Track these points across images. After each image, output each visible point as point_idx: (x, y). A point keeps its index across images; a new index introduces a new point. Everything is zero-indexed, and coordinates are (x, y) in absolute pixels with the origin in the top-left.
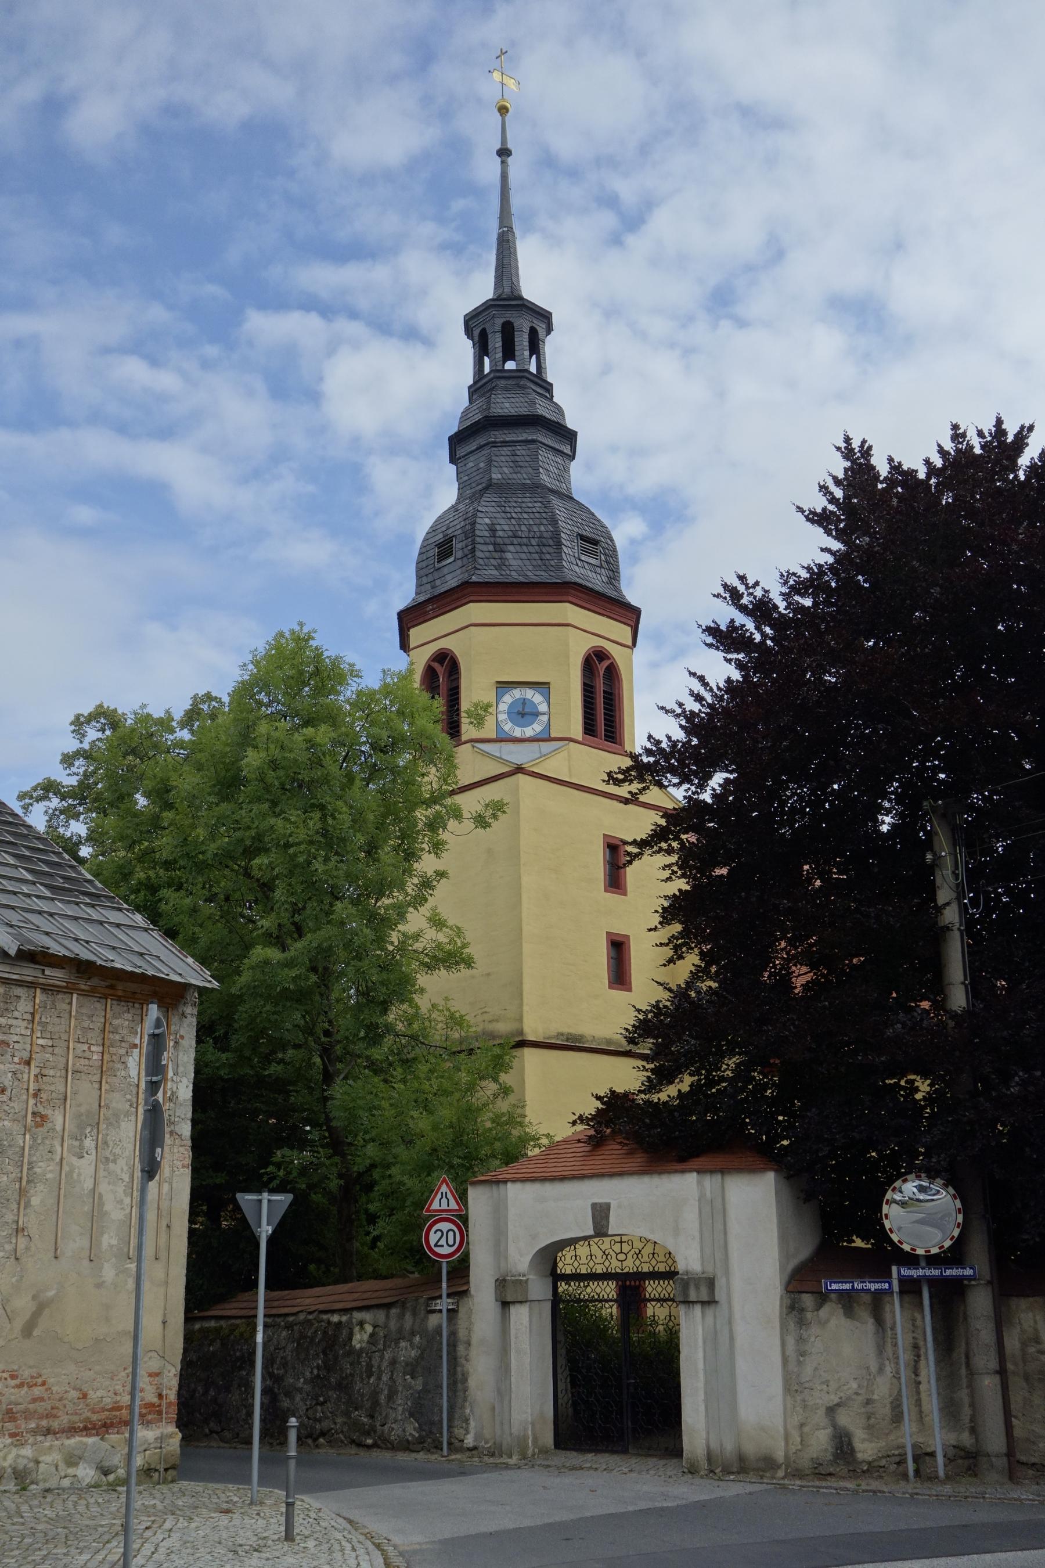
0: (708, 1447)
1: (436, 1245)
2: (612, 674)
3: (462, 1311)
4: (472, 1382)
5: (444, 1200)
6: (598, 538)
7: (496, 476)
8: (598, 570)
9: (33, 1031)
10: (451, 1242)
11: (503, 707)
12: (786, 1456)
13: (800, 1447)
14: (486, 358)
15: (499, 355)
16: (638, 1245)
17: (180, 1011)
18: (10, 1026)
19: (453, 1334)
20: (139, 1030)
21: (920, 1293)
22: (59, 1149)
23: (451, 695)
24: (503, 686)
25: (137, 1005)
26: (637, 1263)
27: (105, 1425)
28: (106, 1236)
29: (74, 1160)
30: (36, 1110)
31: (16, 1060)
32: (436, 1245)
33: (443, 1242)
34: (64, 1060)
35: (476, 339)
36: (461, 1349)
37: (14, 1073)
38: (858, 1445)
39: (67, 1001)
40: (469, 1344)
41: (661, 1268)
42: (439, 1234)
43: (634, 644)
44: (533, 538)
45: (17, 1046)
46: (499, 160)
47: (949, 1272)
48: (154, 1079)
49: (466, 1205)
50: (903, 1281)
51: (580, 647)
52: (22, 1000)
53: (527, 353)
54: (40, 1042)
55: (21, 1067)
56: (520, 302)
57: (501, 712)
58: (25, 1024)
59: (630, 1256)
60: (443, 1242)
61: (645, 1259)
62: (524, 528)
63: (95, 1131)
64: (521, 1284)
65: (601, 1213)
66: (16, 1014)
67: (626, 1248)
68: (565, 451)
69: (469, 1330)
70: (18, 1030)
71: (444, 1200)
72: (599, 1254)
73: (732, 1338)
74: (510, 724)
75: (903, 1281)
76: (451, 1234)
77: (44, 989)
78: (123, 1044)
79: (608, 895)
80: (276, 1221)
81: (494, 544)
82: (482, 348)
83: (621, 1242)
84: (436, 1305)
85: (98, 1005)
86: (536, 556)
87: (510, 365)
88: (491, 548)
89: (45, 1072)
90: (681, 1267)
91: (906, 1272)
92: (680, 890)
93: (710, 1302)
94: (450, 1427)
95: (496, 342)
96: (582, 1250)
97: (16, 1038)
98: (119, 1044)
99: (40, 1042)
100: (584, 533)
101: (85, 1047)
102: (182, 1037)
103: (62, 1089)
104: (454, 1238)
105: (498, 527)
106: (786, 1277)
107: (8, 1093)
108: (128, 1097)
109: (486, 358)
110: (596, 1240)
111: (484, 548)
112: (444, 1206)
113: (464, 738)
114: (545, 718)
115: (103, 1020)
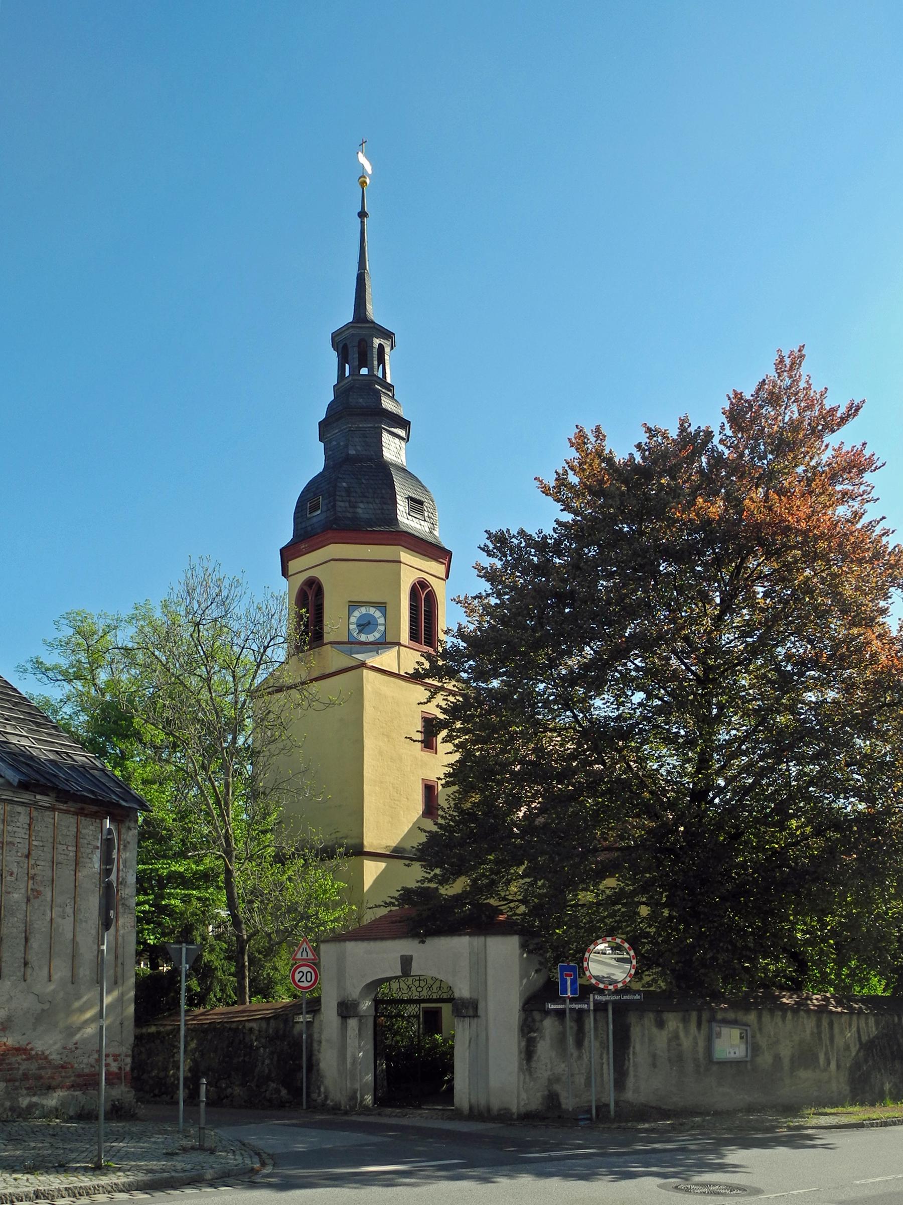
0: (470, 1101)
1: (299, 981)
2: (431, 598)
3: (316, 1024)
4: (322, 1065)
5: (305, 953)
6: (423, 500)
7: (352, 452)
8: (422, 523)
9: (30, 836)
10: (309, 979)
11: (353, 619)
12: (518, 1108)
13: (527, 1102)
14: (347, 365)
15: (356, 363)
16: (430, 982)
17: (127, 825)
18: (15, 832)
19: (310, 1037)
20: (100, 837)
21: (606, 1010)
22: (49, 912)
23: (317, 618)
24: (354, 605)
25: (98, 821)
26: (430, 993)
27: (85, 1085)
28: (82, 969)
29: (60, 920)
30: (33, 887)
31: (19, 854)
32: (299, 981)
33: (304, 979)
34: (51, 856)
35: (340, 351)
36: (315, 1045)
37: (18, 863)
38: (563, 1101)
39: (52, 816)
40: (320, 1042)
41: (445, 996)
42: (301, 974)
43: (447, 577)
44: (377, 498)
45: (19, 845)
46: (359, 220)
47: (625, 997)
48: (108, 867)
49: (319, 955)
50: (597, 1003)
51: (407, 580)
52: (22, 815)
53: (376, 363)
54: (35, 843)
55: (23, 859)
56: (372, 325)
57: (352, 623)
58: (24, 831)
59: (425, 988)
60: (304, 979)
61: (435, 990)
62: (370, 491)
63: (73, 902)
64: (355, 1005)
65: (406, 962)
66: (18, 824)
67: (422, 984)
68: (402, 435)
69: (320, 1033)
70: (20, 835)
71: (305, 953)
72: (405, 987)
73: (487, 1039)
74: (371, 613)
75: (597, 1003)
76: (309, 974)
77: (37, 809)
78: (89, 846)
79: (423, 753)
80: (192, 961)
81: (350, 502)
82: (343, 359)
83: (420, 980)
84: (299, 1018)
85: (72, 820)
86: (379, 512)
87: (364, 371)
88: (347, 504)
89: (38, 863)
90: (457, 995)
91: (598, 997)
92: (451, 765)
93: (476, 1015)
94: (308, 1095)
95: (354, 355)
96: (395, 985)
97: (18, 840)
98: (86, 846)
99: (35, 843)
100: (414, 496)
101: (65, 847)
102: (129, 843)
103: (50, 874)
104: (311, 977)
105: (352, 490)
106: (523, 1000)
107: (15, 875)
108: (94, 881)
109: (347, 365)
110: (404, 979)
111: (342, 504)
112: (305, 956)
113: (325, 641)
114: (382, 628)
115: (76, 830)
